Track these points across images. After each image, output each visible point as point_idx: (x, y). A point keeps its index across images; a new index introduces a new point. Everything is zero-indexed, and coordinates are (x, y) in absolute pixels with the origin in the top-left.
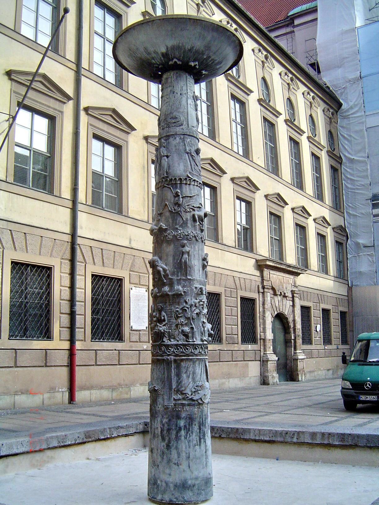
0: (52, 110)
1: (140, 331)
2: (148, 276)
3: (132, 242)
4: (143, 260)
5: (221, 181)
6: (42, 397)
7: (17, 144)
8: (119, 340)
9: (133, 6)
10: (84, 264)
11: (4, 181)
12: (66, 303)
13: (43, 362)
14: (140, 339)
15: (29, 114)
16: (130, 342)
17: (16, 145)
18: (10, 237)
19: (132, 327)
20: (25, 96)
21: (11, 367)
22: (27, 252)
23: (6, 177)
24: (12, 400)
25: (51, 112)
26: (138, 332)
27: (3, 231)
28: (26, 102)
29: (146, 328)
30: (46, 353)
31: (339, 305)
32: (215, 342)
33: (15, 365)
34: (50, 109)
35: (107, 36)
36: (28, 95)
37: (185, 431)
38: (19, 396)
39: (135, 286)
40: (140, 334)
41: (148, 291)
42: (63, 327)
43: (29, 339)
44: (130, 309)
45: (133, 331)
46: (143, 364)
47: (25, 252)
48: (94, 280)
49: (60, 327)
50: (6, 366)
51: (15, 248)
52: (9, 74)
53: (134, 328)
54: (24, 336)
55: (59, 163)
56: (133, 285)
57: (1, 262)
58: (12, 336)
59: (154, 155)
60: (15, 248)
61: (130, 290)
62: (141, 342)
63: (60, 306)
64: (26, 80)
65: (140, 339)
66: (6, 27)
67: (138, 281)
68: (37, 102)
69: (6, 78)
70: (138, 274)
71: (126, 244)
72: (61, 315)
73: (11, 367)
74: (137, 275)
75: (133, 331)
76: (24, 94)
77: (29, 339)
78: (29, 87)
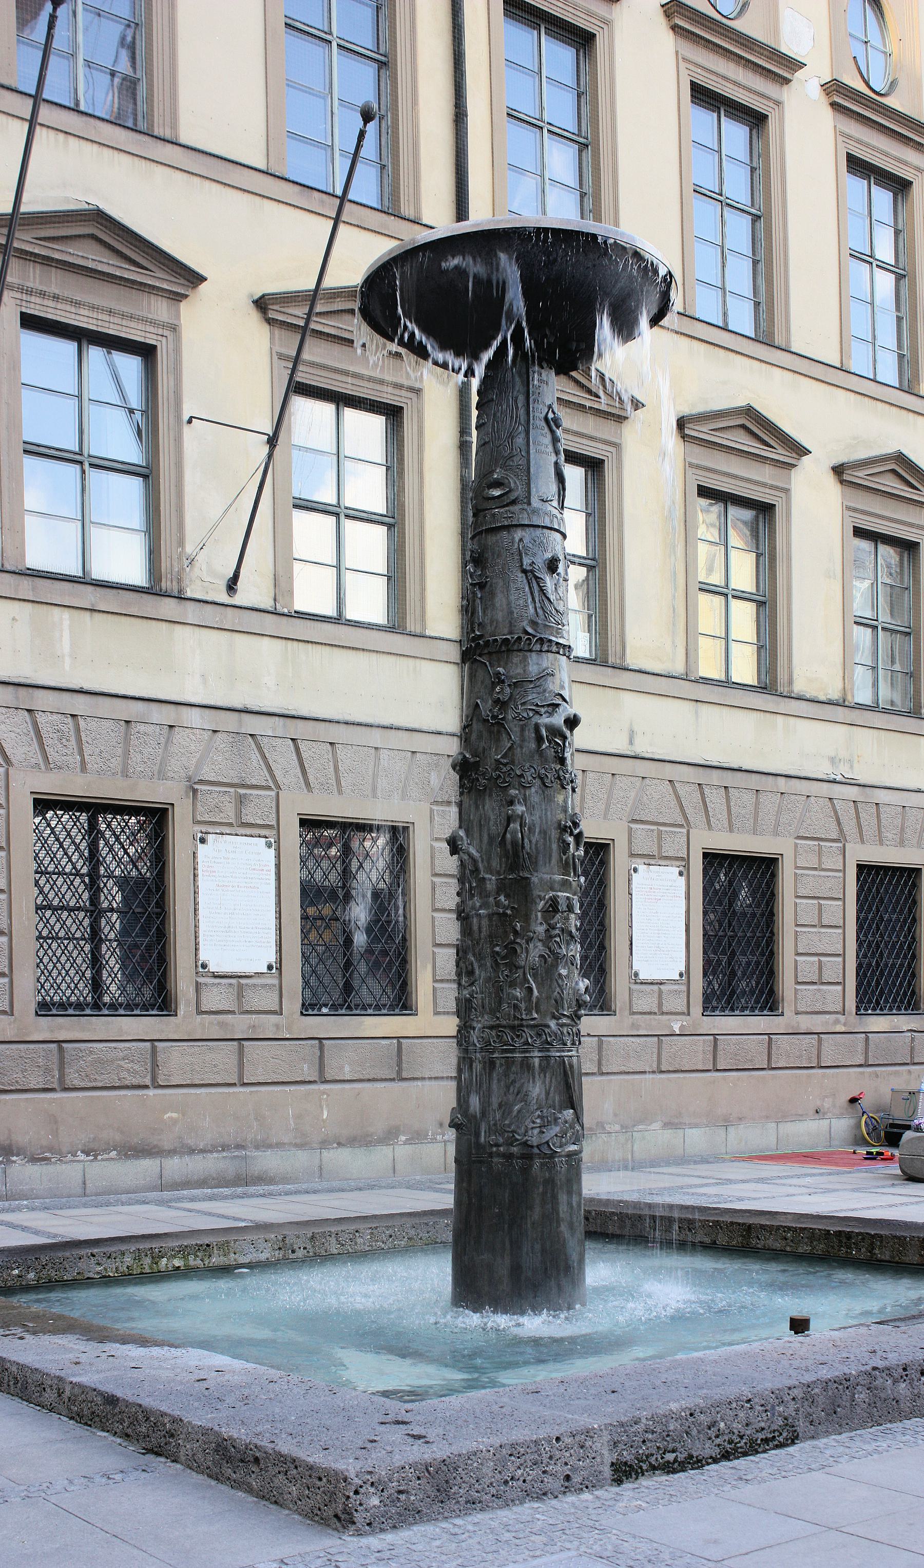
0: (390, 390)
1: (661, 984)
2: (684, 831)
3: (638, 740)
4: (670, 788)
5: (790, 483)
6: (391, 1155)
7: (298, 502)
8: (602, 1009)
9: (799, 74)
10: (273, 793)
11: (268, 612)
12: (449, 919)
13: (48, 1071)
14: (660, 1005)
15: (327, 409)
16: (200, 1012)
17: (296, 506)
18: (295, 758)
19: (636, 974)
20: (297, 360)
21: (310, 1082)
22: (340, 792)
23: (275, 600)
24: (317, 1162)
25: (388, 396)
26: (655, 987)
27: (274, 744)
28: (304, 375)
29: (681, 975)
30: (400, 1045)
31: (696, 817)
32: (899, 1009)
33: (239, 1081)
34: (385, 388)
35: (728, 191)
36: (305, 356)
37: (136, 1314)
38: (332, 1151)
39: (646, 861)
40: (660, 992)
41: (685, 873)
42: (442, 981)
43: (355, 1012)
44: (631, 927)
45: (642, 983)
46: (669, 1072)
47: (336, 792)
48: (709, 863)
49: (435, 981)
50: (298, 1079)
51: (307, 784)
52: (262, 304)
53: (642, 976)
54: (341, 1006)
55: (417, 543)
56: (639, 860)
57: (3, 802)
58: (312, 1006)
59: (563, 441)
60: (307, 784)
61: (630, 875)
62: (663, 1013)
63: (433, 926)
64: (36, 239)
65: (660, 1005)
66: (240, 164)
67: (655, 848)
68: (346, 373)
69: (254, 316)
70: (655, 827)
71: (619, 745)
72: (436, 950)
73: (310, 1082)
74: (653, 831)
75: (642, 983)
76: (294, 354)
77: (355, 1012)
78: (304, 331)
